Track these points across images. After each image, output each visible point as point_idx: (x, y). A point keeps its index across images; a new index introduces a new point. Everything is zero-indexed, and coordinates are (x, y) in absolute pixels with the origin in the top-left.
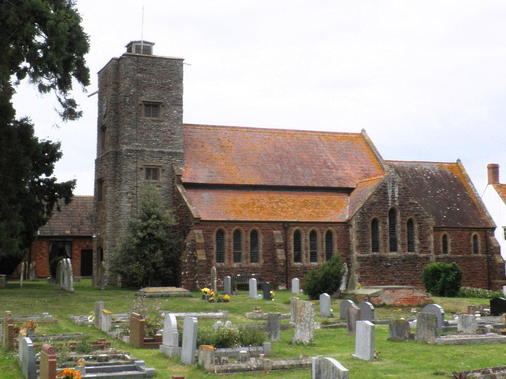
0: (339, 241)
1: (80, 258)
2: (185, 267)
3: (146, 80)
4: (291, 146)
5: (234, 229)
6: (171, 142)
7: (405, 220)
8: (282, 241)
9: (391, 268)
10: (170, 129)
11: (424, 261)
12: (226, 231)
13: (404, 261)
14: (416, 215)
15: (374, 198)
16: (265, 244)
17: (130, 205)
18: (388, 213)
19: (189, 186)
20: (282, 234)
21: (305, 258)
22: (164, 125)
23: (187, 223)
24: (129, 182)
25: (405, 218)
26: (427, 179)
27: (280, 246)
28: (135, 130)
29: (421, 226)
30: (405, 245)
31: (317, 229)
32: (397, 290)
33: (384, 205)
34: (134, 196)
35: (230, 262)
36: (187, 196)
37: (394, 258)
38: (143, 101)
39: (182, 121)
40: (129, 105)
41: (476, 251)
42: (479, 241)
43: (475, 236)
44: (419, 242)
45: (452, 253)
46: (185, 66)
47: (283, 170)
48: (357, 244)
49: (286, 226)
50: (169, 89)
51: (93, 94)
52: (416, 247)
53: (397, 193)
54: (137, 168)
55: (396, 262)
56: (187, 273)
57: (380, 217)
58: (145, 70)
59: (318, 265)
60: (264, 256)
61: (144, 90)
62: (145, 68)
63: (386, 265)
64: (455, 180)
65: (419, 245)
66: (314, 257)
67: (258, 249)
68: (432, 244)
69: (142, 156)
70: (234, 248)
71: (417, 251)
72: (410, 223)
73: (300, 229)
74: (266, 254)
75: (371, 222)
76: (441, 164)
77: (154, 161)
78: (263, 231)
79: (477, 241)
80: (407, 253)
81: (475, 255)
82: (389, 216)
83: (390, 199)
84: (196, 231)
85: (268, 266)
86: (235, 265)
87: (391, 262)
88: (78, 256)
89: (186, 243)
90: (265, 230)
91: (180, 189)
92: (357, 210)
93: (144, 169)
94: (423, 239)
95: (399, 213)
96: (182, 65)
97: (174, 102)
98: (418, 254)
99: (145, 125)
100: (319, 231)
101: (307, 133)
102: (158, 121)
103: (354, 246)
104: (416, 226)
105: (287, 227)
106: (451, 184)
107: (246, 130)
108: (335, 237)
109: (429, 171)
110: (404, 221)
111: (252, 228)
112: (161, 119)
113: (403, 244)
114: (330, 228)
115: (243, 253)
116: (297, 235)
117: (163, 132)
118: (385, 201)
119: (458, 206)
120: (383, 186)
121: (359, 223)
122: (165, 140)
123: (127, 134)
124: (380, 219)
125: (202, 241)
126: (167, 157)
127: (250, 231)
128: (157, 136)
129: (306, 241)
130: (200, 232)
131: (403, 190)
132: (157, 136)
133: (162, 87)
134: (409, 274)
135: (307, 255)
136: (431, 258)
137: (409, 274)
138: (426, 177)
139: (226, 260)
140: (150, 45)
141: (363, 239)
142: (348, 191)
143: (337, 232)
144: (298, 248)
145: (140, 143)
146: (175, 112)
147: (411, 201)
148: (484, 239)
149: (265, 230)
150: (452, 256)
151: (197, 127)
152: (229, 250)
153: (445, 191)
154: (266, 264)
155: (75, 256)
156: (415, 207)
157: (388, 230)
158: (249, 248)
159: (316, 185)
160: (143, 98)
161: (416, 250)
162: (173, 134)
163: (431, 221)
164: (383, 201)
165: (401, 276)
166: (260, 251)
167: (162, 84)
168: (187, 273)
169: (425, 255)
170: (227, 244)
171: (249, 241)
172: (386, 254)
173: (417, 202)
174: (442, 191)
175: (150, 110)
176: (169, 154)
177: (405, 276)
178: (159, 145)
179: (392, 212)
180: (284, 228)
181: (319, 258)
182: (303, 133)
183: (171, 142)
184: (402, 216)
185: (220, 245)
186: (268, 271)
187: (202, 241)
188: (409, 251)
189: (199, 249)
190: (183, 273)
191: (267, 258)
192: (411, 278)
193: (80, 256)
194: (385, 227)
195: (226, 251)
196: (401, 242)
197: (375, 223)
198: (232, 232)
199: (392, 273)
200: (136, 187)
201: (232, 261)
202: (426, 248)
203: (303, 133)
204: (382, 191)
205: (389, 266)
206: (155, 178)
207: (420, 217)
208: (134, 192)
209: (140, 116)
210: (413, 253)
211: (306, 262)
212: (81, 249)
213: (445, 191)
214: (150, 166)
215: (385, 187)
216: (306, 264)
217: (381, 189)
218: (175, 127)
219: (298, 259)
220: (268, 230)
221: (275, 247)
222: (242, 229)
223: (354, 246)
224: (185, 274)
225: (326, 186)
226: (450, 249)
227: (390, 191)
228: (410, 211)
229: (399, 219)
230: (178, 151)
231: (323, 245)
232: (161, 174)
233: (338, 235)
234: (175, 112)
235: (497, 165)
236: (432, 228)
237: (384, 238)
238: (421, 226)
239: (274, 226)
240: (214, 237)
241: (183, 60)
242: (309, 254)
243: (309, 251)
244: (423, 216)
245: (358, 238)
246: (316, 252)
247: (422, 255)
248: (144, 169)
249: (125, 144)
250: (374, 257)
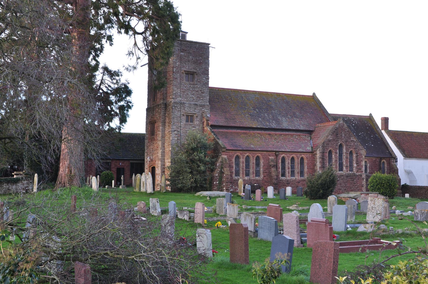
0: (308, 164)
2: (216, 179)
3: (186, 57)
5: (246, 155)
6: (201, 98)
12: (241, 156)
13: (347, 177)
16: (264, 165)
17: (176, 139)
21: (288, 174)
22: (197, 87)
24: (176, 123)
29: (357, 155)
30: (348, 167)
31: (285, 156)
34: (179, 133)
35: (243, 176)
38: (185, 71)
39: (208, 84)
40: (176, 73)
42: (386, 166)
43: (383, 162)
44: (356, 166)
46: (210, 49)
48: (320, 166)
49: (277, 154)
50: (200, 63)
51: (145, 65)
52: (354, 168)
56: (217, 182)
59: (296, 179)
60: (263, 172)
61: (185, 64)
64: (369, 127)
65: (356, 167)
67: (260, 169)
68: (364, 167)
69: (184, 107)
72: (351, 153)
73: (285, 156)
75: (328, 152)
77: (191, 110)
80: (349, 172)
82: (339, 149)
84: (223, 156)
85: (266, 179)
90: (265, 156)
93: (185, 116)
96: (208, 48)
99: (185, 87)
100: (296, 158)
102: (194, 84)
103: (318, 168)
104: (355, 155)
105: (278, 155)
108: (306, 161)
110: (348, 152)
111: (257, 155)
112: (196, 83)
113: (347, 167)
114: (303, 156)
115: (251, 171)
116: (283, 160)
117: (197, 92)
121: (321, 152)
124: (333, 150)
126: (199, 108)
127: (255, 156)
128: (193, 94)
129: (289, 163)
132: (193, 94)
135: (289, 172)
140: (185, 33)
143: (307, 158)
144: (283, 168)
145: (182, 98)
146: (204, 78)
147: (352, 139)
149: (265, 156)
154: (265, 178)
157: (338, 158)
159: (290, 128)
160: (184, 69)
161: (354, 170)
162: (203, 93)
165: (345, 186)
166: (261, 169)
168: (217, 182)
169: (360, 173)
170: (241, 165)
171: (255, 163)
175: (189, 77)
176: (201, 106)
178: (194, 100)
180: (276, 155)
181: (296, 174)
183: (201, 98)
184: (346, 149)
185: (237, 164)
186: (266, 182)
188: (350, 171)
190: (215, 183)
191: (266, 174)
193: (116, 172)
195: (241, 169)
197: (330, 152)
198: (245, 157)
199: (340, 184)
200: (180, 127)
201: (244, 175)
202: (360, 169)
206: (192, 121)
208: (179, 130)
209: (183, 81)
210: (353, 172)
211: (288, 177)
212: (116, 167)
214: (189, 113)
216: (288, 178)
218: (204, 88)
219: (283, 175)
220: (266, 156)
221: (271, 167)
222: (250, 155)
223: (318, 168)
224: (216, 183)
225: (297, 129)
229: (344, 150)
232: (195, 119)
233: (307, 160)
235: (388, 118)
236: (364, 157)
238: (357, 155)
239: (270, 153)
240: (234, 160)
241: (209, 44)
243: (290, 170)
245: (320, 162)
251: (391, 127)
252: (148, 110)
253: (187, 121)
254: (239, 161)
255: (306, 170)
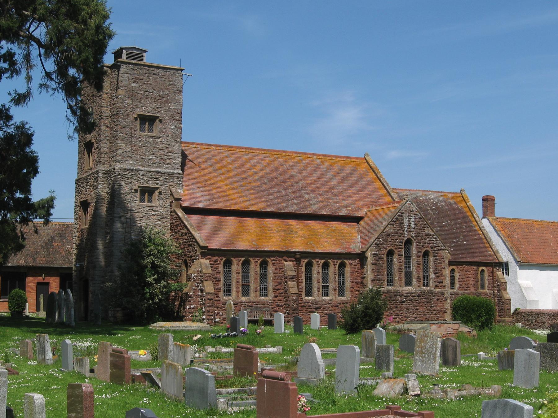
1: (36, 291)
4: (293, 169)
6: (168, 161)
7: (421, 252)
8: (294, 273)
9: (406, 303)
10: (167, 146)
11: (438, 296)
13: (419, 296)
14: (432, 248)
15: (390, 228)
18: (403, 244)
19: (189, 211)
20: (294, 265)
21: (317, 292)
23: (190, 252)
25: (420, 250)
26: (432, 210)
27: (292, 278)
28: (129, 146)
32: (443, 325)
33: (400, 236)
36: (189, 220)
37: (410, 294)
38: (139, 115)
41: (483, 287)
45: (460, 288)
47: (288, 196)
48: (373, 277)
52: (431, 281)
53: (413, 223)
54: (131, 189)
55: (412, 298)
57: (396, 249)
58: (141, 79)
59: (330, 300)
61: (140, 102)
62: (142, 77)
63: (401, 301)
66: (325, 290)
70: (242, 281)
71: (431, 287)
72: (426, 254)
74: (276, 288)
76: (445, 194)
78: (274, 262)
79: (484, 276)
81: (482, 291)
83: (406, 229)
86: (244, 299)
87: (406, 297)
88: (32, 289)
89: (191, 274)
91: (180, 213)
92: (372, 240)
94: (438, 273)
95: (415, 245)
97: (172, 116)
98: (433, 288)
101: (309, 156)
103: (369, 280)
104: (431, 259)
106: (455, 215)
107: (244, 150)
109: (434, 201)
115: (331, 288)
117: (160, 150)
118: (401, 232)
119: (464, 239)
120: (399, 216)
121: (374, 254)
122: (162, 159)
123: (120, 151)
124: (395, 250)
125: (210, 271)
128: (153, 154)
130: (207, 261)
131: (419, 220)
133: (158, 100)
134: (424, 310)
136: (446, 293)
137: (424, 310)
138: (431, 207)
139: (234, 294)
141: (378, 272)
142: (357, 220)
147: (427, 232)
148: (491, 274)
150: (460, 292)
151: (191, 146)
152: (237, 282)
153: (451, 222)
155: (30, 290)
156: (431, 238)
157: (403, 263)
158: (259, 281)
160: (138, 111)
161: (431, 284)
162: (170, 152)
163: (447, 255)
164: (399, 231)
167: (159, 96)
171: (259, 272)
172: (401, 289)
173: (432, 233)
174: (448, 223)
176: (167, 174)
177: (419, 312)
179: (409, 242)
182: (305, 156)
183: (168, 161)
184: (418, 248)
187: (210, 271)
188: (424, 286)
189: (206, 280)
190: (188, 307)
192: (426, 315)
193: (35, 289)
194: (400, 259)
196: (416, 276)
199: (407, 309)
203: (305, 156)
204: (397, 220)
205: (404, 302)
207: (435, 249)
210: (429, 288)
213: (451, 222)
215: (402, 216)
216: (318, 299)
217: (397, 219)
219: (309, 293)
223: (369, 280)
226: (457, 285)
227: (406, 221)
228: (426, 243)
229: (414, 250)
230: (176, 171)
231: (335, 278)
234: (173, 127)
236: (447, 261)
237: (399, 271)
242: (321, 288)
243: (321, 284)
244: (439, 248)
245: (373, 271)
246: (328, 286)
247: (437, 290)
248: (139, 191)
249: (119, 162)
250: (389, 291)
251: (500, 211)
252: (77, 182)
253: (142, 200)
254: (311, 270)
255: (348, 284)
